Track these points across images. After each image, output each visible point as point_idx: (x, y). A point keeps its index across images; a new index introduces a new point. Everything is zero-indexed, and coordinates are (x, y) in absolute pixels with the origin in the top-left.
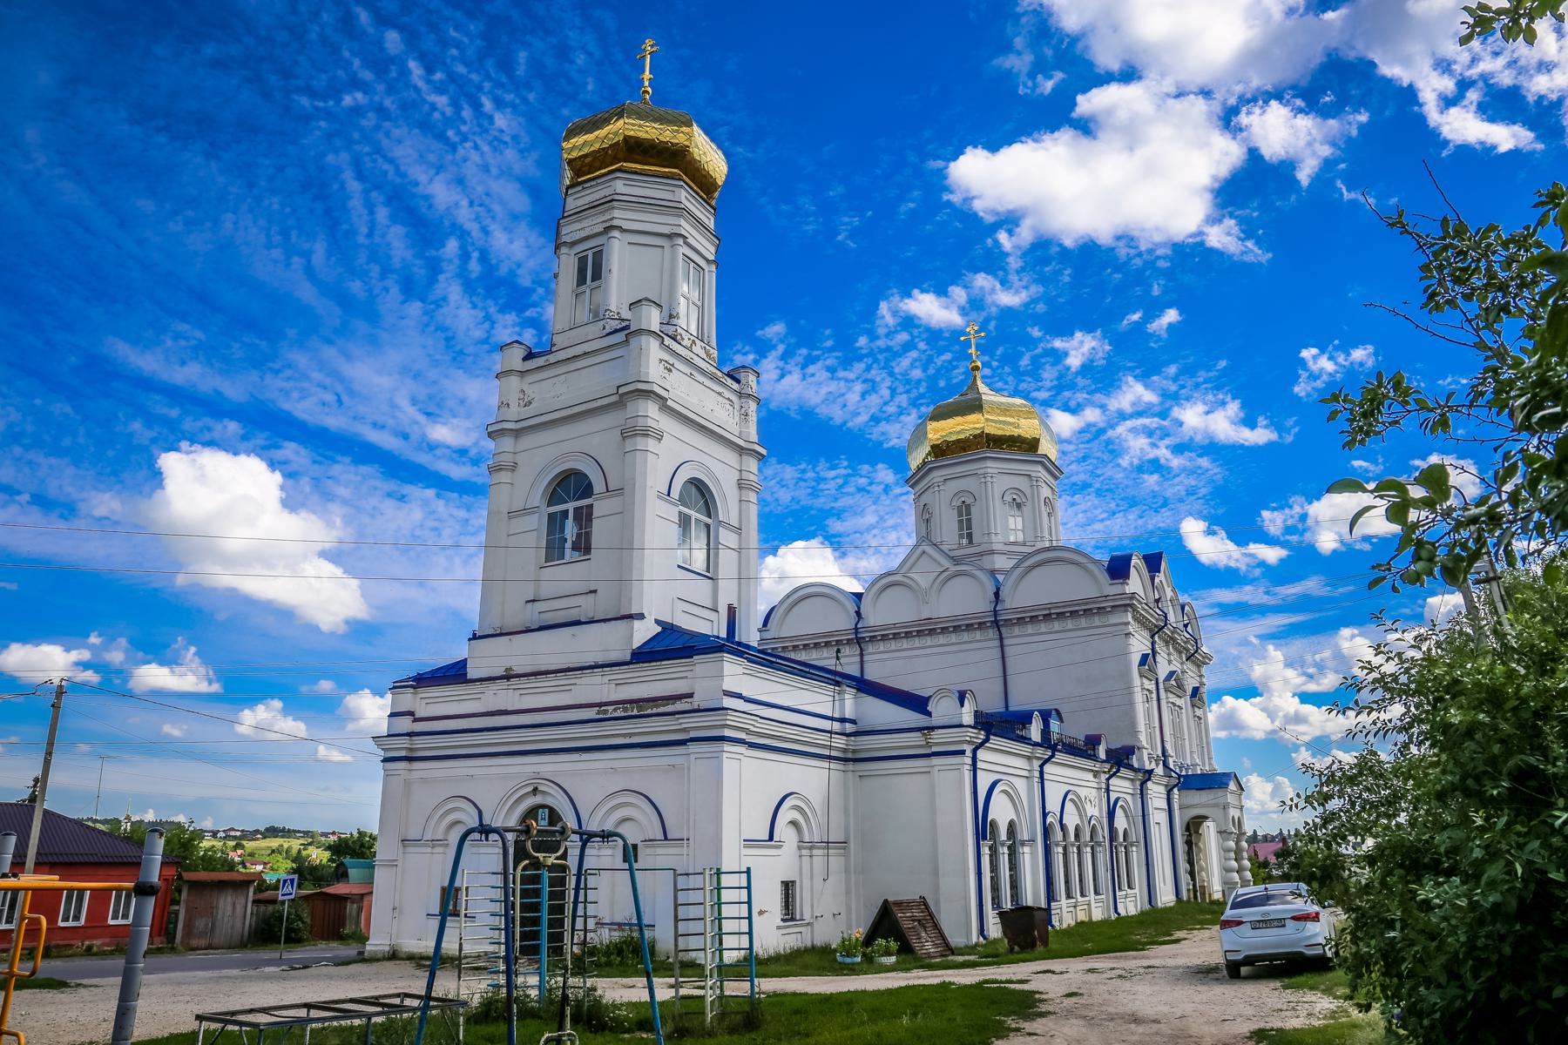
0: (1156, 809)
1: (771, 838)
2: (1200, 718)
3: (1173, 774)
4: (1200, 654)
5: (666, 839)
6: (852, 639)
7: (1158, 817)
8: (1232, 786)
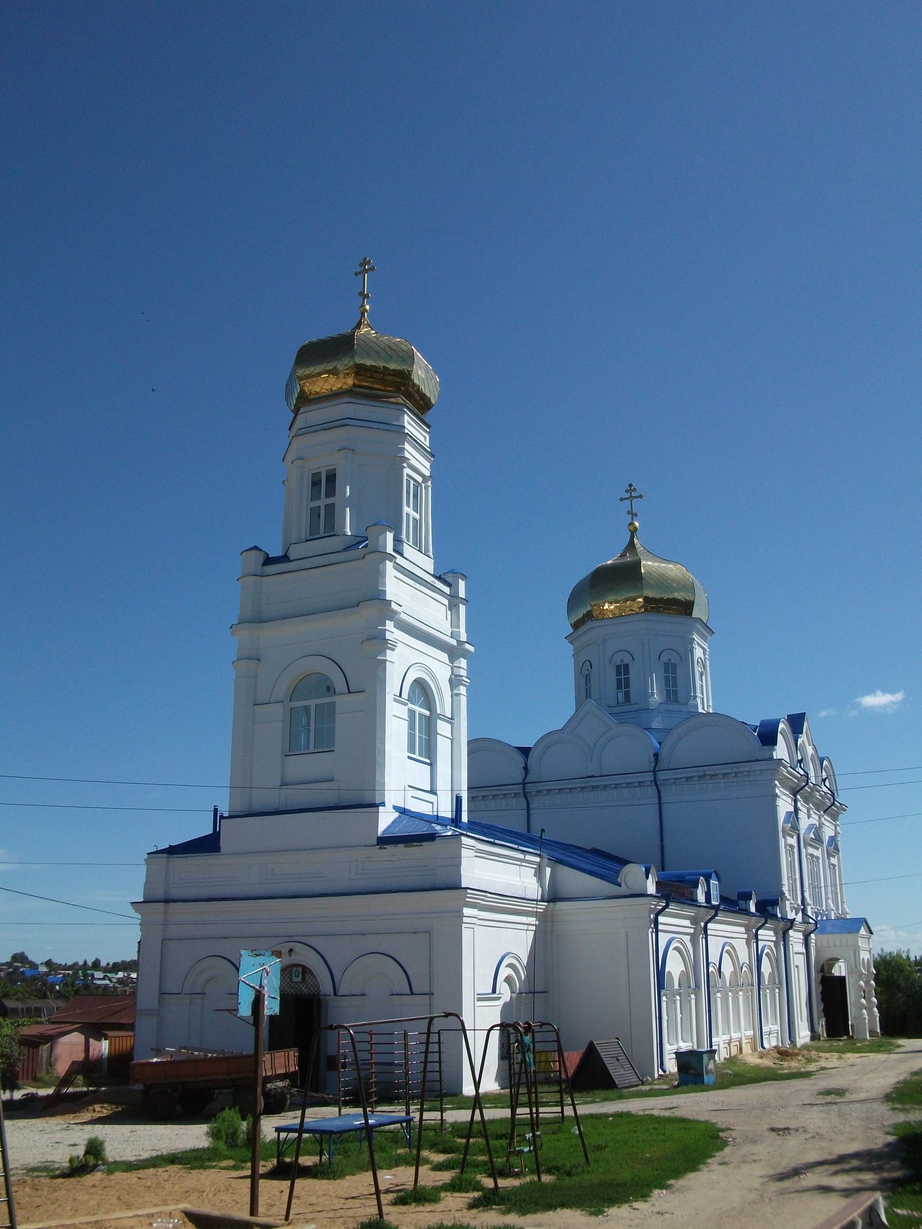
0: (796, 953)
1: (494, 991)
2: (834, 866)
3: (811, 921)
4: (836, 807)
5: (412, 993)
6: (520, 793)
7: (798, 961)
8: (863, 931)
